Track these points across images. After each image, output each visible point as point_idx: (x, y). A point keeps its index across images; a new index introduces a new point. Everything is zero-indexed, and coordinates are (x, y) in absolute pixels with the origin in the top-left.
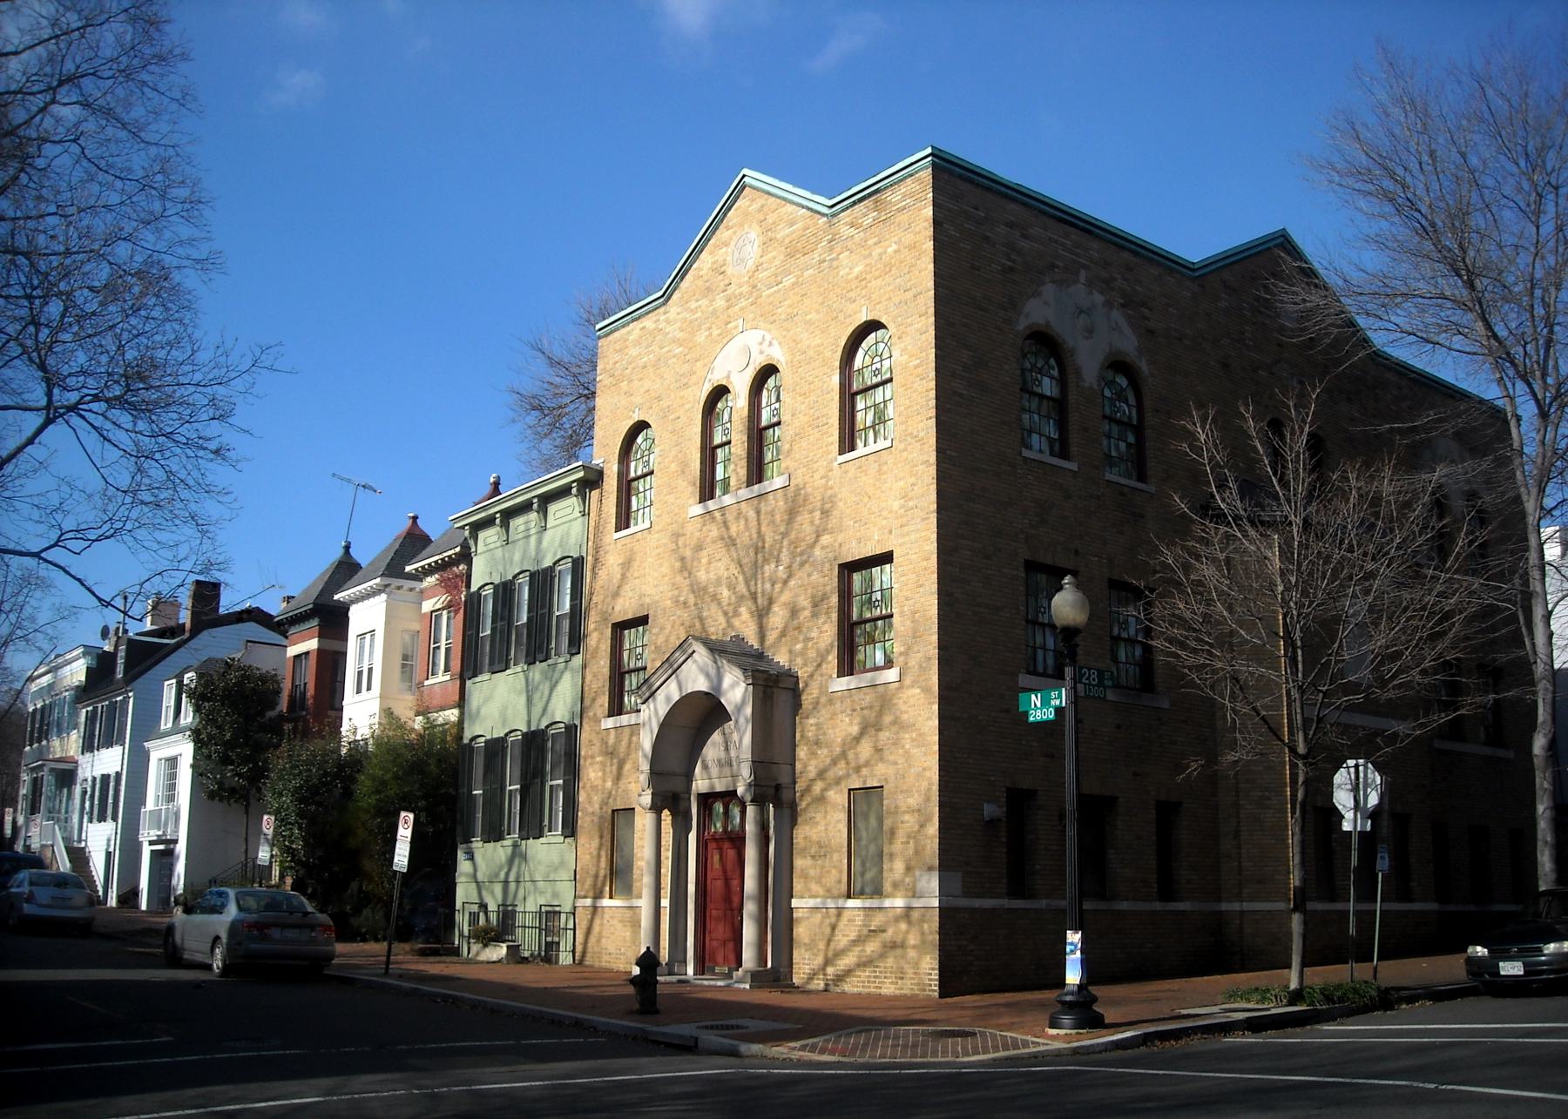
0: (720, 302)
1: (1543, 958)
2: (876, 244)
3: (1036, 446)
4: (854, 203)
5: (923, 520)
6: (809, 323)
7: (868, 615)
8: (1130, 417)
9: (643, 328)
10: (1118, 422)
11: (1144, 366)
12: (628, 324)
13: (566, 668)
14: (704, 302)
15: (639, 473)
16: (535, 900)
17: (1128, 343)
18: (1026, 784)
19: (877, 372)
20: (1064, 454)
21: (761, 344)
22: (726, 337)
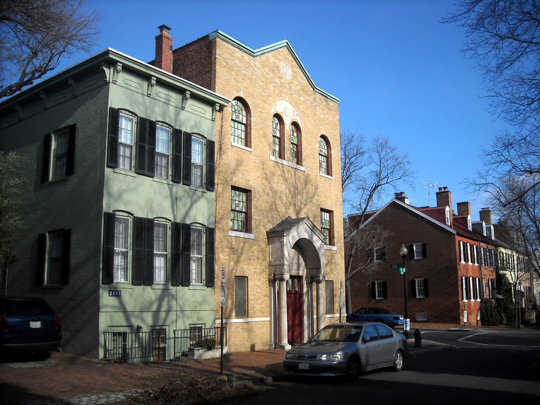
1: (335, 362)
4: (321, 94)
12: (235, 47)
13: (202, 196)
16: (184, 322)
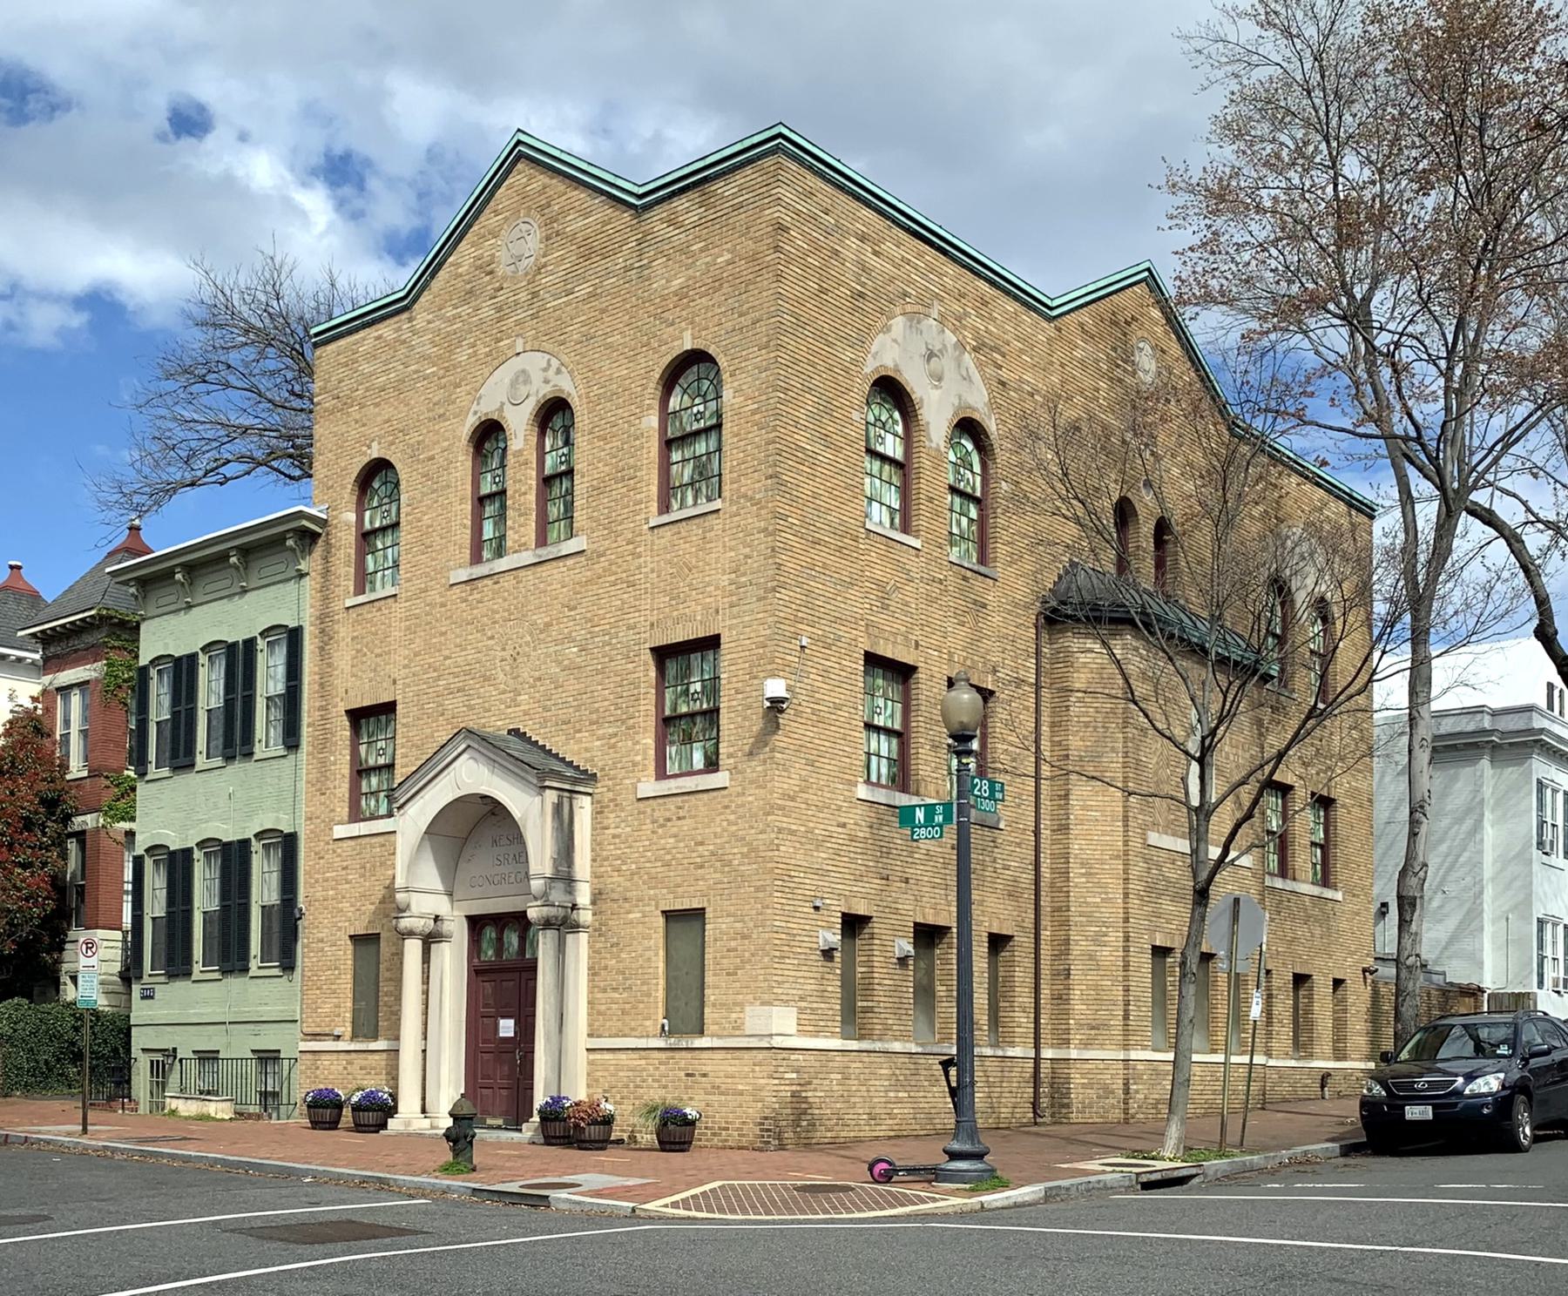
0: (487, 312)
2: (702, 250)
3: (876, 519)
5: (759, 600)
6: (609, 346)
7: (684, 709)
8: (974, 488)
9: (378, 338)
10: (961, 494)
11: (991, 426)
14: (465, 310)
15: (377, 525)
17: (979, 402)
18: (861, 909)
19: (699, 416)
20: (906, 528)
21: (545, 370)
22: (497, 360)
